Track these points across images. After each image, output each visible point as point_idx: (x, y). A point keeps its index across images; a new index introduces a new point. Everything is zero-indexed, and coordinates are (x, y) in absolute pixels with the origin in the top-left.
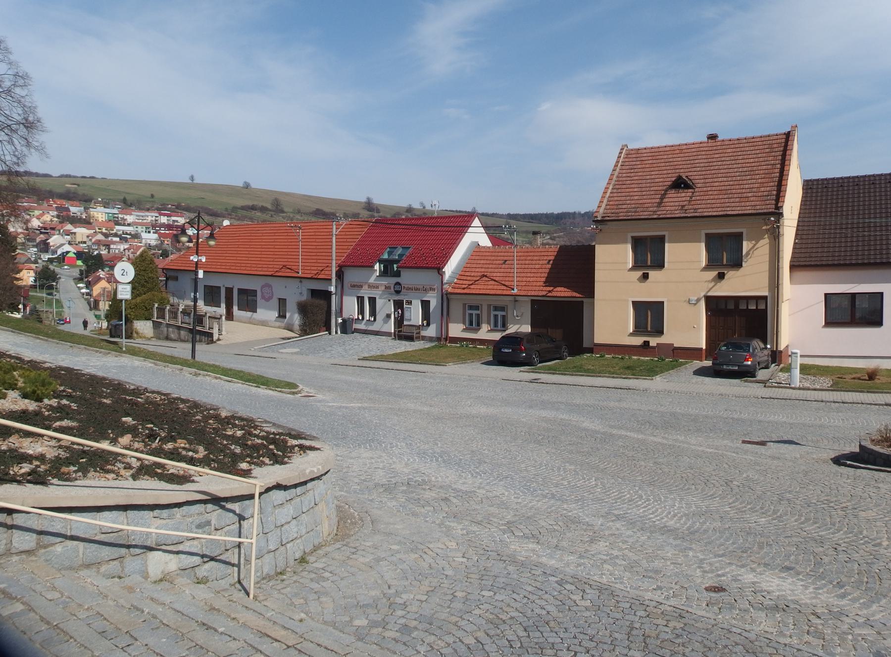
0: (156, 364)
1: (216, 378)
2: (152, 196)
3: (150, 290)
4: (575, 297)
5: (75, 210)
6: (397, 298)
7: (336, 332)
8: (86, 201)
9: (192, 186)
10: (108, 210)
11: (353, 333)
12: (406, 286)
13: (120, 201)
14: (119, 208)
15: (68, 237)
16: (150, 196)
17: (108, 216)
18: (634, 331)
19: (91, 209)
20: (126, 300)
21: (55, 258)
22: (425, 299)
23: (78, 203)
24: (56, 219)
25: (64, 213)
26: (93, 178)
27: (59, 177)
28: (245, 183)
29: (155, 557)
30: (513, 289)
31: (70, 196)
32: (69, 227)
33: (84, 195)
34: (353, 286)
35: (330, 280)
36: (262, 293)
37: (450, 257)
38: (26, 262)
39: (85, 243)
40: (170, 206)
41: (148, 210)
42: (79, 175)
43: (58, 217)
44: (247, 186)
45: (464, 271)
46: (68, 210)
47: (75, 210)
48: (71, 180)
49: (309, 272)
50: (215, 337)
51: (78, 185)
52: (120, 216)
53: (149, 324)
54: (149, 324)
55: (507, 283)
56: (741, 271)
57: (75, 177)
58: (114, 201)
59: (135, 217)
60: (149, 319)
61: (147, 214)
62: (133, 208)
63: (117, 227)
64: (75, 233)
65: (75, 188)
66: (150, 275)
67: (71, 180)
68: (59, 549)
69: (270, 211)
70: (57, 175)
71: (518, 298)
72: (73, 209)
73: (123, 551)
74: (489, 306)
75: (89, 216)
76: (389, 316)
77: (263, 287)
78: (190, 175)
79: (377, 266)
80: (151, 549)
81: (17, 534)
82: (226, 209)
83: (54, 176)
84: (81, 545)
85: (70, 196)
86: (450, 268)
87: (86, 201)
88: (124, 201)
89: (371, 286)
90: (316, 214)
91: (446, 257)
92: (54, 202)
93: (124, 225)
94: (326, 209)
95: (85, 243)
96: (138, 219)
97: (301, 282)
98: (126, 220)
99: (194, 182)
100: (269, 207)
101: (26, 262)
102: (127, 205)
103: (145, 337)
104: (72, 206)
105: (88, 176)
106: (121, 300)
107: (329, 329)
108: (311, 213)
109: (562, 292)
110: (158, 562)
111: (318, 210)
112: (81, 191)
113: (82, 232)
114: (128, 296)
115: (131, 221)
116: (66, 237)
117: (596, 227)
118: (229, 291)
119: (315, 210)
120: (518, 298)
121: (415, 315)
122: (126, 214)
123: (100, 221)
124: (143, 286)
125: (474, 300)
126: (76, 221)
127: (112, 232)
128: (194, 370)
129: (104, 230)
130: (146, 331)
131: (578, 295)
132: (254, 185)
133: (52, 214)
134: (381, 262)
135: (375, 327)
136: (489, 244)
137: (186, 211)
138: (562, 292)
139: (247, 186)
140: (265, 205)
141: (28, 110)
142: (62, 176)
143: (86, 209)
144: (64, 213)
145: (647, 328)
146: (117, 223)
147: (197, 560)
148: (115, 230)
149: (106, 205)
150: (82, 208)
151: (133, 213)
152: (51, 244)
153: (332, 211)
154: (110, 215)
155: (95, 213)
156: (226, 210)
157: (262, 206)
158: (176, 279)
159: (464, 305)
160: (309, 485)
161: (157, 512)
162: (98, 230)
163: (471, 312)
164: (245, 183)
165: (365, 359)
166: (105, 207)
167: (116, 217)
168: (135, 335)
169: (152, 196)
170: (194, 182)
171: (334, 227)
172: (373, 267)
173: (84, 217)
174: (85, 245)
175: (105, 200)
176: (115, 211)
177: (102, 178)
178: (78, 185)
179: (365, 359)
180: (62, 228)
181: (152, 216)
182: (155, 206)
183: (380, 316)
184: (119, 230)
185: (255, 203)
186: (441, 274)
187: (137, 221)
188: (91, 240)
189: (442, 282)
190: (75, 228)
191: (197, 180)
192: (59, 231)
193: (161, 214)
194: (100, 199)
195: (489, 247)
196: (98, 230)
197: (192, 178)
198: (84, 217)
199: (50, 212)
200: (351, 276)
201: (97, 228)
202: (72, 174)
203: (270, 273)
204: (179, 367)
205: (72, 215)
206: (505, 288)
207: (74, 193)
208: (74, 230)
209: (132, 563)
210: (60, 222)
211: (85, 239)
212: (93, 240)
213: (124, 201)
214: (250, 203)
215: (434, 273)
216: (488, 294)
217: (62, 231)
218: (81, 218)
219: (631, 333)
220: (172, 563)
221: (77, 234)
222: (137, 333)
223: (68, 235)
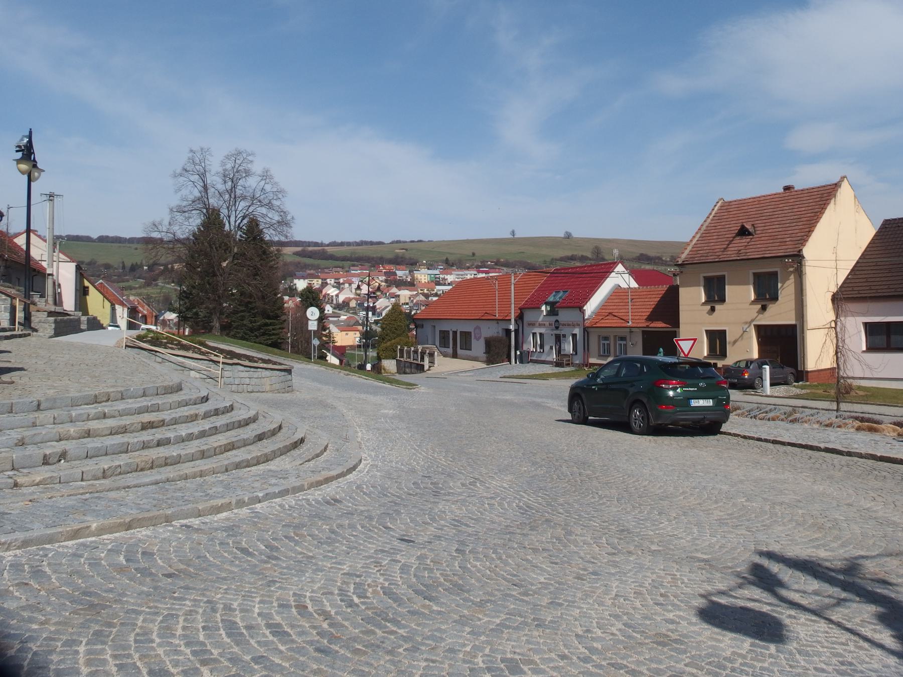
0: (326, 369)
1: (359, 377)
2: (474, 254)
3: (399, 335)
4: (668, 327)
5: (401, 274)
6: (558, 332)
7: (516, 363)
8: (412, 264)
9: (513, 241)
10: (430, 272)
11: (528, 363)
12: (562, 323)
13: (442, 261)
14: (441, 269)
15: (393, 300)
16: (471, 254)
17: (430, 277)
18: (708, 355)
19: (415, 272)
20: (314, 331)
21: (381, 320)
22: (574, 333)
23: (404, 267)
24: (383, 284)
25: (392, 278)
26: (420, 241)
27: (390, 243)
28: (567, 232)
29: (192, 373)
30: (629, 322)
31: (398, 261)
32: (394, 290)
33: (410, 259)
34: (529, 324)
35: (510, 320)
36: (475, 334)
37: (590, 299)
38: (354, 325)
39: (407, 304)
40: (489, 263)
41: (468, 268)
42: (408, 240)
43: (386, 281)
44: (568, 236)
45: (605, 310)
46: (395, 274)
47: (401, 274)
48: (401, 245)
49: (476, 315)
50: (426, 367)
51: (406, 250)
52: (441, 276)
53: (394, 362)
54: (394, 362)
55: (624, 318)
56: (829, 296)
57: (405, 242)
58: (437, 262)
59: (455, 276)
60: (394, 358)
61: (467, 272)
62: (455, 268)
63: (438, 287)
64: (399, 296)
65: (403, 254)
66: (399, 324)
67: (401, 245)
68: (167, 364)
69: (590, 260)
70: (389, 242)
71: (633, 330)
72: (400, 273)
73: (183, 368)
74: (615, 336)
75: (413, 279)
76: (551, 348)
77: (475, 329)
78: (511, 230)
79: (543, 308)
80: (192, 370)
81: (157, 357)
82: (545, 261)
83: (408, 241)
84: (173, 364)
85: (398, 261)
86: (591, 306)
87: (412, 264)
88: (447, 262)
89: (541, 325)
90: (639, 260)
91: (587, 298)
92: (384, 267)
93: (445, 285)
94: (652, 253)
95: (407, 304)
96: (458, 278)
97: (498, 323)
98: (447, 279)
99: (515, 236)
100: (589, 255)
101: (354, 325)
102: (449, 265)
103: (390, 373)
104: (399, 270)
105: (416, 240)
106: (311, 331)
107: (510, 361)
108: (634, 259)
109: (659, 325)
110: (193, 373)
111: (642, 255)
112: (408, 255)
113: (405, 294)
114: (315, 328)
115: (452, 280)
116: (392, 299)
117: (792, 261)
118: (455, 333)
119: (638, 255)
120: (633, 330)
121: (568, 348)
122: (447, 274)
123: (423, 282)
124: (394, 333)
125: (604, 333)
126: (401, 284)
127: (433, 292)
128: (347, 372)
129: (426, 291)
130: (391, 368)
131: (664, 325)
132: (575, 235)
133: (381, 279)
134: (547, 304)
135: (543, 358)
136: (634, 284)
137: (505, 267)
138: (659, 325)
139: (568, 236)
140: (585, 254)
141: (283, 213)
142: (392, 243)
143: (411, 272)
144: (392, 278)
145: (716, 353)
146: (438, 284)
147: (205, 377)
148: (435, 290)
149: (430, 267)
150: (408, 272)
151: (453, 272)
152: (377, 307)
153: (658, 255)
154: (432, 276)
155: (419, 276)
156: (545, 262)
157: (582, 256)
158: (422, 326)
159: (599, 336)
160: (259, 370)
161: (194, 360)
162: (420, 292)
163: (604, 342)
164: (567, 232)
165: (504, 377)
166: (428, 269)
167: (437, 278)
168: (383, 371)
169: (474, 254)
170: (515, 236)
171: (513, 277)
172: (539, 308)
173: (409, 280)
174: (407, 306)
175: (429, 262)
176: (437, 272)
177: (429, 241)
178: (406, 250)
179: (504, 377)
180: (388, 291)
181: (471, 275)
182: (476, 264)
183: (547, 348)
184: (440, 290)
185: (575, 253)
186: (583, 312)
187: (457, 280)
188: (412, 301)
189: (584, 318)
190: (400, 290)
191: (518, 235)
192: (386, 294)
193: (479, 272)
194: (425, 262)
195: (636, 288)
196: (420, 292)
197: (513, 233)
198: (409, 280)
199: (380, 277)
200: (529, 316)
201: (419, 290)
202: (402, 239)
203: (478, 318)
204: (339, 370)
205: (398, 278)
206: (624, 322)
207: (402, 258)
208: (399, 293)
209: (186, 373)
210: (388, 286)
211: (407, 301)
212: (415, 301)
213: (447, 262)
214: (569, 253)
215: (577, 311)
216: (623, 327)
217: (388, 294)
218: (406, 281)
219: (705, 357)
220: (198, 375)
221: (401, 296)
222: (384, 369)
223: (393, 298)
